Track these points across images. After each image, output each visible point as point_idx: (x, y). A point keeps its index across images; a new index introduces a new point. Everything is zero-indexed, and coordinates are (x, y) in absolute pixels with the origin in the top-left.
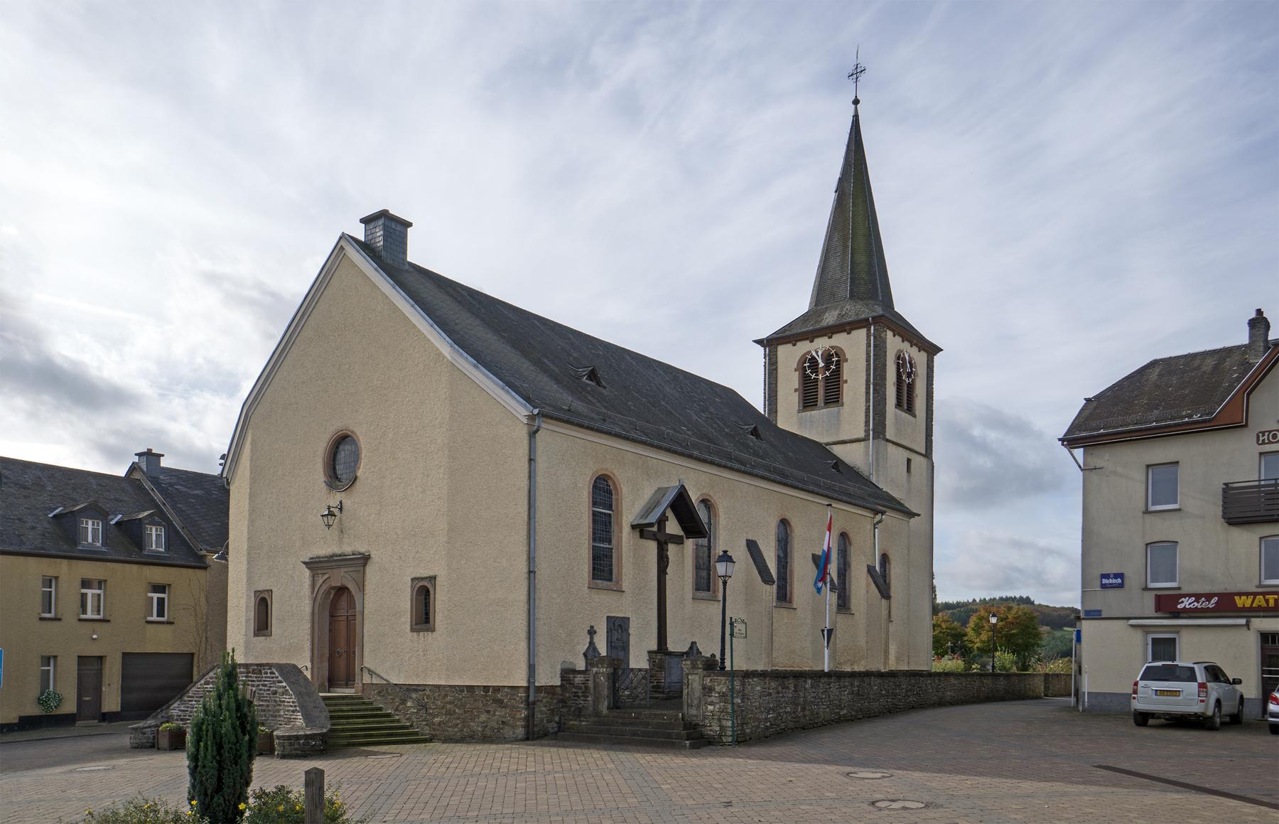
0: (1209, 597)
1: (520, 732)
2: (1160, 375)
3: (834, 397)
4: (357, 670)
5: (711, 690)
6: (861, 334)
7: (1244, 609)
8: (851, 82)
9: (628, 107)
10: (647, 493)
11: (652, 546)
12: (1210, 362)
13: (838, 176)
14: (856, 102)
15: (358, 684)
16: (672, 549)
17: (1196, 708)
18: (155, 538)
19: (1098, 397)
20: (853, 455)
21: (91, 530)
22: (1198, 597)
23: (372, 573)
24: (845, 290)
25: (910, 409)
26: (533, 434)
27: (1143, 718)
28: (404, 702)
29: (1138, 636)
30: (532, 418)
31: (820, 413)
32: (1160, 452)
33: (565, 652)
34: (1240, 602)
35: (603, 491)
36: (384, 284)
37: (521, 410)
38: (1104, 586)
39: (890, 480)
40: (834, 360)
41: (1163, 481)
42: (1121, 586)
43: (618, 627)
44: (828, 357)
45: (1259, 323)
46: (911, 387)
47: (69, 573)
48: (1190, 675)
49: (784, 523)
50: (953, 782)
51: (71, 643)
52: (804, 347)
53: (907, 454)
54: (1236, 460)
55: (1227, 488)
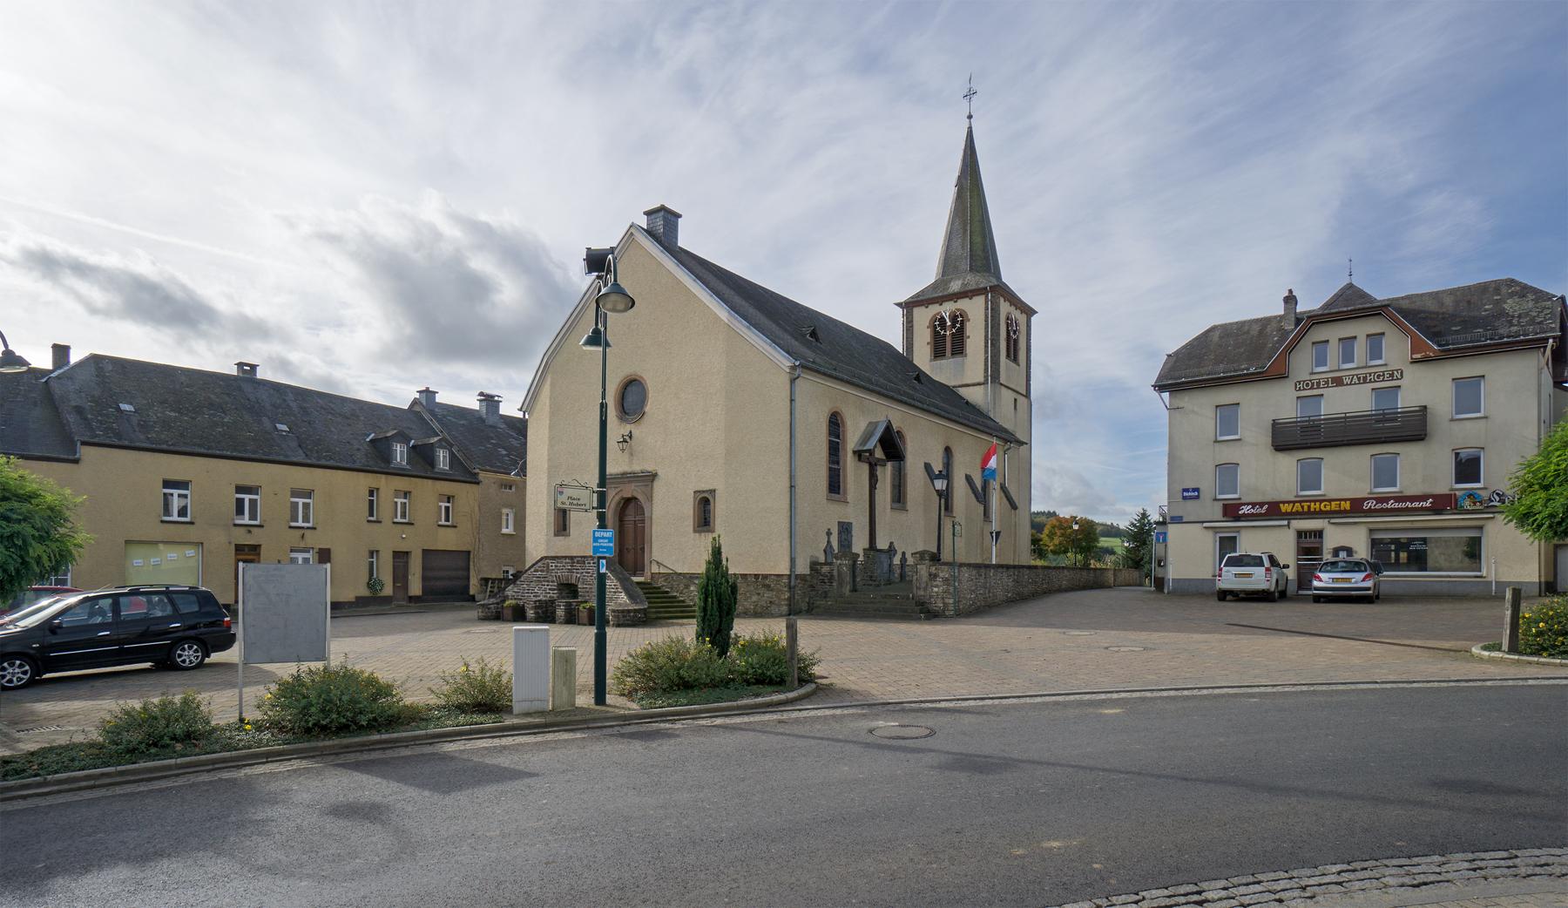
0: (1261, 505)
1: (785, 609)
2: (1221, 338)
3: (959, 348)
4: (647, 562)
5: (936, 576)
6: (979, 301)
7: (1287, 514)
8: (966, 101)
9: (690, 85)
10: (863, 425)
11: (866, 467)
12: (1256, 328)
13: (957, 174)
14: (970, 117)
15: (648, 573)
16: (879, 470)
17: (1263, 586)
18: (442, 459)
19: (1177, 353)
20: (975, 395)
21: (400, 452)
22: (1254, 505)
23: (659, 487)
24: (965, 265)
25: (1015, 360)
26: (793, 381)
27: (1224, 595)
28: (687, 587)
29: (1210, 534)
30: (793, 368)
31: (948, 363)
32: (1227, 396)
33: (813, 549)
34: (1284, 508)
35: (835, 424)
36: (669, 263)
37: (786, 362)
38: (1185, 498)
39: (1004, 415)
40: (959, 320)
41: (1228, 417)
42: (1197, 497)
43: (845, 529)
44: (954, 318)
45: (1290, 300)
46: (1016, 341)
47: (387, 486)
48: (1258, 562)
49: (948, 450)
50: (1156, 637)
51: (388, 540)
52: (934, 309)
53: (1014, 395)
54: (1281, 402)
55: (1275, 423)
